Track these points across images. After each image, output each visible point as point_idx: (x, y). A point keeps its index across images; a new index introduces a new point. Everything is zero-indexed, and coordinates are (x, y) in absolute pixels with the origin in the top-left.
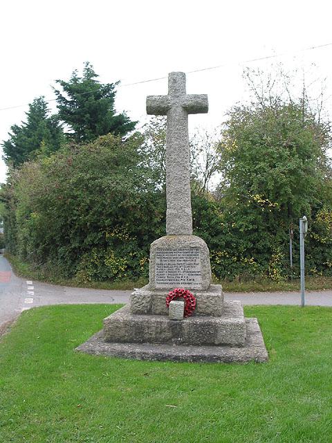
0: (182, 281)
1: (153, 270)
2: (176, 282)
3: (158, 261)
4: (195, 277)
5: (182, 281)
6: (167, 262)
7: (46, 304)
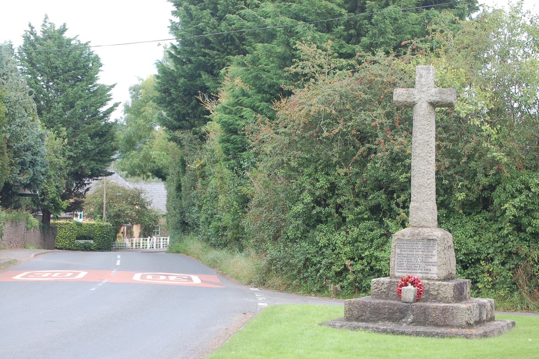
0: (420, 271)
1: (393, 259)
2: (414, 271)
3: (398, 251)
4: (431, 268)
5: (420, 271)
6: (406, 253)
7: (432, 205)
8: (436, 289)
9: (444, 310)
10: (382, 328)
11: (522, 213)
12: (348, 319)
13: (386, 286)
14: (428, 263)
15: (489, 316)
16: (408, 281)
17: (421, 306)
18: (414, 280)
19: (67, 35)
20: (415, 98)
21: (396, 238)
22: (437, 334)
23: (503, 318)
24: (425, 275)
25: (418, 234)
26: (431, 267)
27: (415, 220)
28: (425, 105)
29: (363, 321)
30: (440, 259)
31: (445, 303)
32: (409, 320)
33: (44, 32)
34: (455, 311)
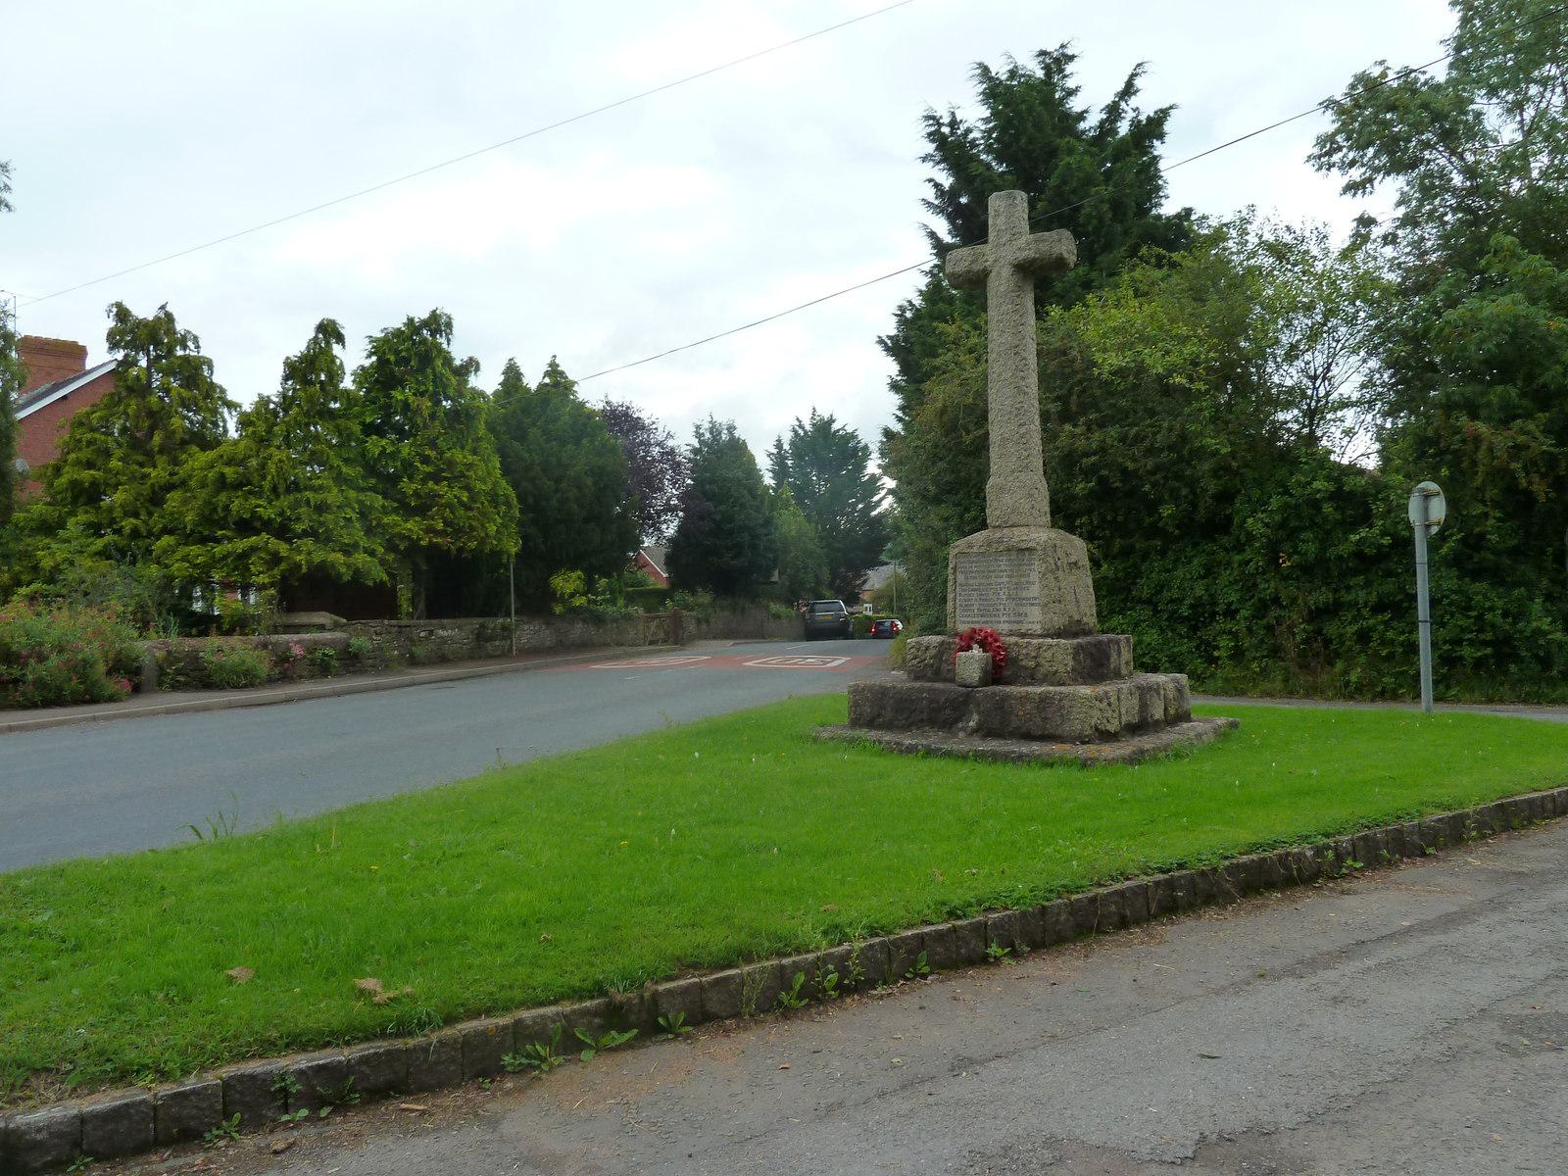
0: (1005, 618)
5: (1005, 618)
6: (977, 581)
8: (1033, 654)
9: (1044, 701)
10: (907, 742)
11: (1281, 534)
12: (855, 723)
13: (933, 652)
14: (1021, 601)
15: (1172, 712)
16: (972, 638)
17: (994, 693)
18: (986, 638)
19: (835, 426)
20: (986, 261)
21: (956, 551)
22: (1020, 757)
23: (1210, 711)
24: (1015, 627)
25: (1000, 541)
26: (1028, 609)
27: (997, 513)
28: (1007, 272)
29: (880, 727)
30: (1046, 591)
31: (1052, 685)
32: (971, 724)
33: (814, 425)
34: (1066, 702)
